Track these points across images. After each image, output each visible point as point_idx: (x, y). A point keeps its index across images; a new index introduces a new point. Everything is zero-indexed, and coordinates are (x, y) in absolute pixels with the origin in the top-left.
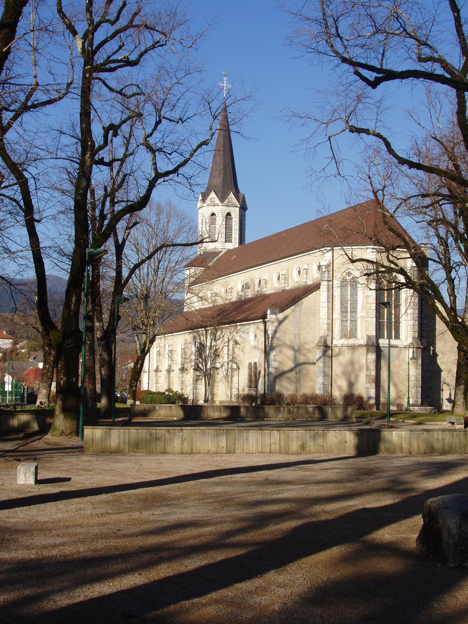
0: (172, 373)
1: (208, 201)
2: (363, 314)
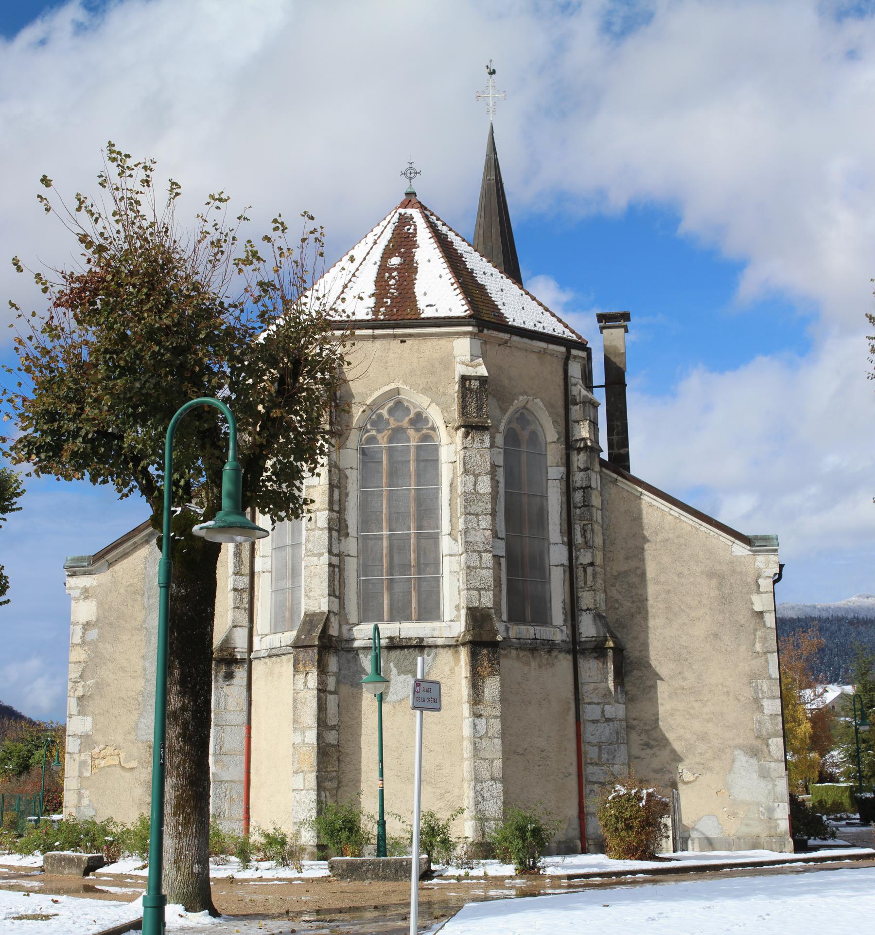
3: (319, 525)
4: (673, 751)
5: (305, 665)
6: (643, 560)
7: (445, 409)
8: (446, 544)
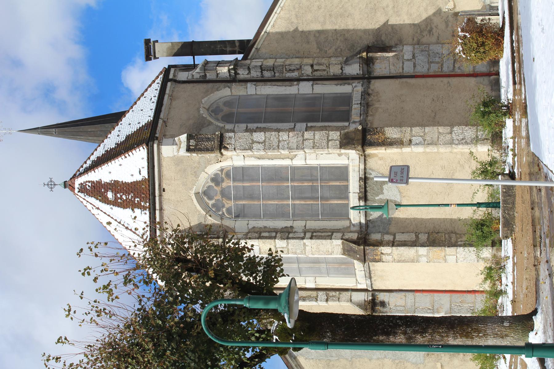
3: (285, 246)
4: (434, 14)
5: (377, 255)
6: (309, 32)
7: (209, 163)
8: (298, 162)
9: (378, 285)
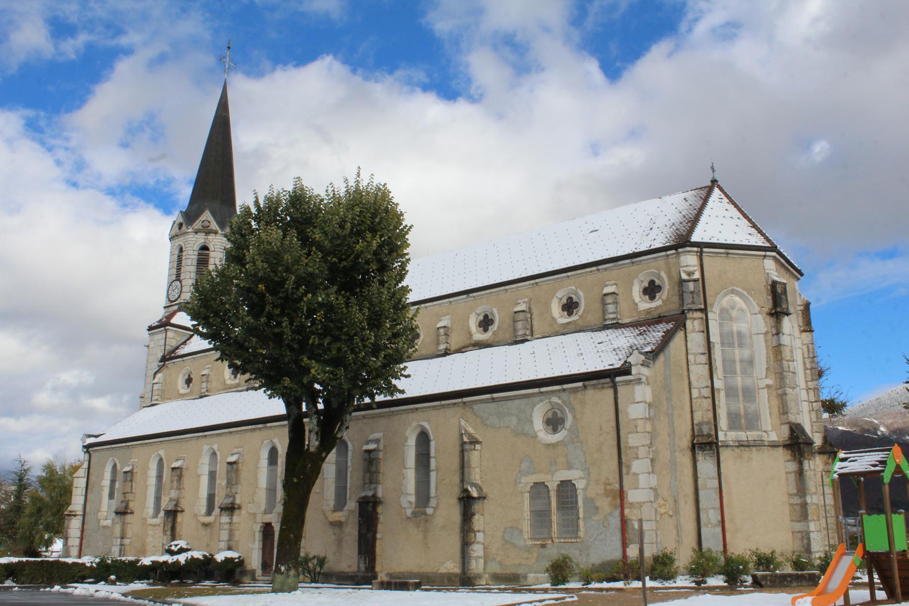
0: (179, 514)
1: (198, 224)
2: (770, 382)
9: (725, 454)
